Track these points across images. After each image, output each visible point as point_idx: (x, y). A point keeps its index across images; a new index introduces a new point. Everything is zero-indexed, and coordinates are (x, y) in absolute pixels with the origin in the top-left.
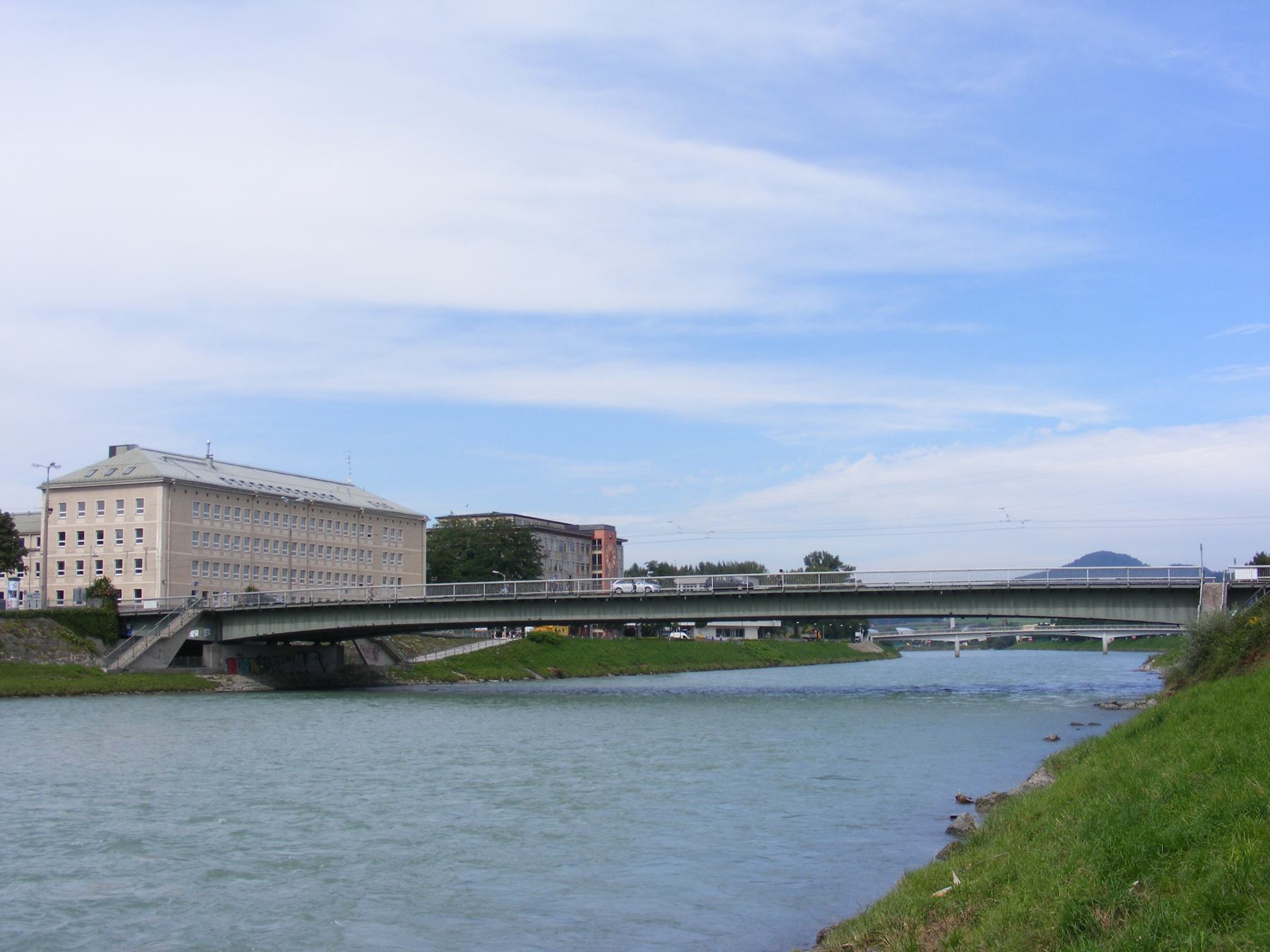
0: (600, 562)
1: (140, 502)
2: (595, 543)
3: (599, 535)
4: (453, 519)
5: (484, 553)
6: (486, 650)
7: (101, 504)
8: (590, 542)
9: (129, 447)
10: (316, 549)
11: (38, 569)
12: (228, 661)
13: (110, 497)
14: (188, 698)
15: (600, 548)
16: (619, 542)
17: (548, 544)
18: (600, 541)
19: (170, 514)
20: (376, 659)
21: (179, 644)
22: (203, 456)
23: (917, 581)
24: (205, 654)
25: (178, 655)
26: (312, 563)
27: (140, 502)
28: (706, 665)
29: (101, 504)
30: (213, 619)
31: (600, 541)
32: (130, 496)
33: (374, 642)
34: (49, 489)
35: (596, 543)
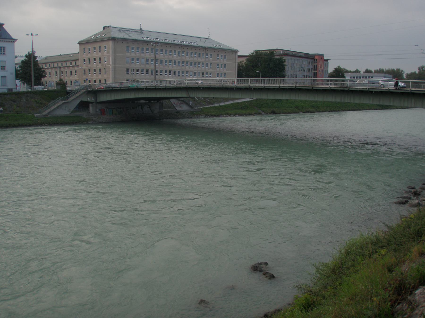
0: (316, 68)
1: (105, 47)
2: (315, 61)
3: (316, 58)
4: (256, 52)
5: (267, 64)
6: (232, 104)
7: (95, 48)
8: (313, 60)
9: (108, 27)
10: (185, 63)
11: (56, 74)
12: (101, 110)
13: (97, 45)
14: (55, 128)
15: (317, 63)
16: (327, 60)
17: (288, 62)
18: (317, 60)
19: (115, 51)
20: (181, 107)
21: (78, 102)
22: (139, 29)
23: (176, 33)
24: (91, 108)
25: (76, 107)
26: (207, 69)
27: (105, 47)
28: (311, 109)
29: (95, 48)
30: (95, 93)
31: (317, 60)
32: (103, 45)
33: (180, 100)
34: (81, 43)
35: (316, 61)
